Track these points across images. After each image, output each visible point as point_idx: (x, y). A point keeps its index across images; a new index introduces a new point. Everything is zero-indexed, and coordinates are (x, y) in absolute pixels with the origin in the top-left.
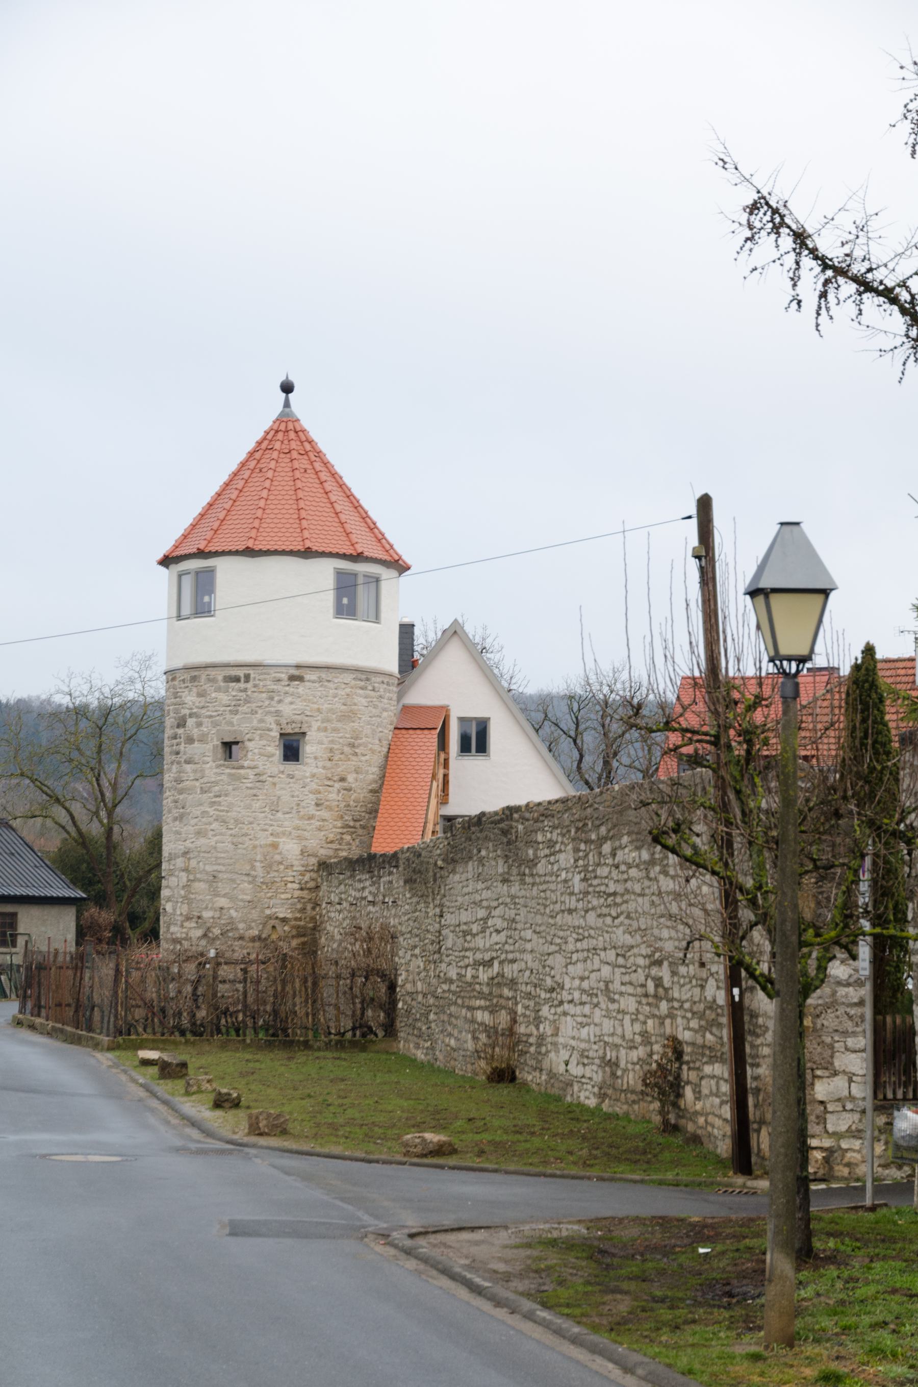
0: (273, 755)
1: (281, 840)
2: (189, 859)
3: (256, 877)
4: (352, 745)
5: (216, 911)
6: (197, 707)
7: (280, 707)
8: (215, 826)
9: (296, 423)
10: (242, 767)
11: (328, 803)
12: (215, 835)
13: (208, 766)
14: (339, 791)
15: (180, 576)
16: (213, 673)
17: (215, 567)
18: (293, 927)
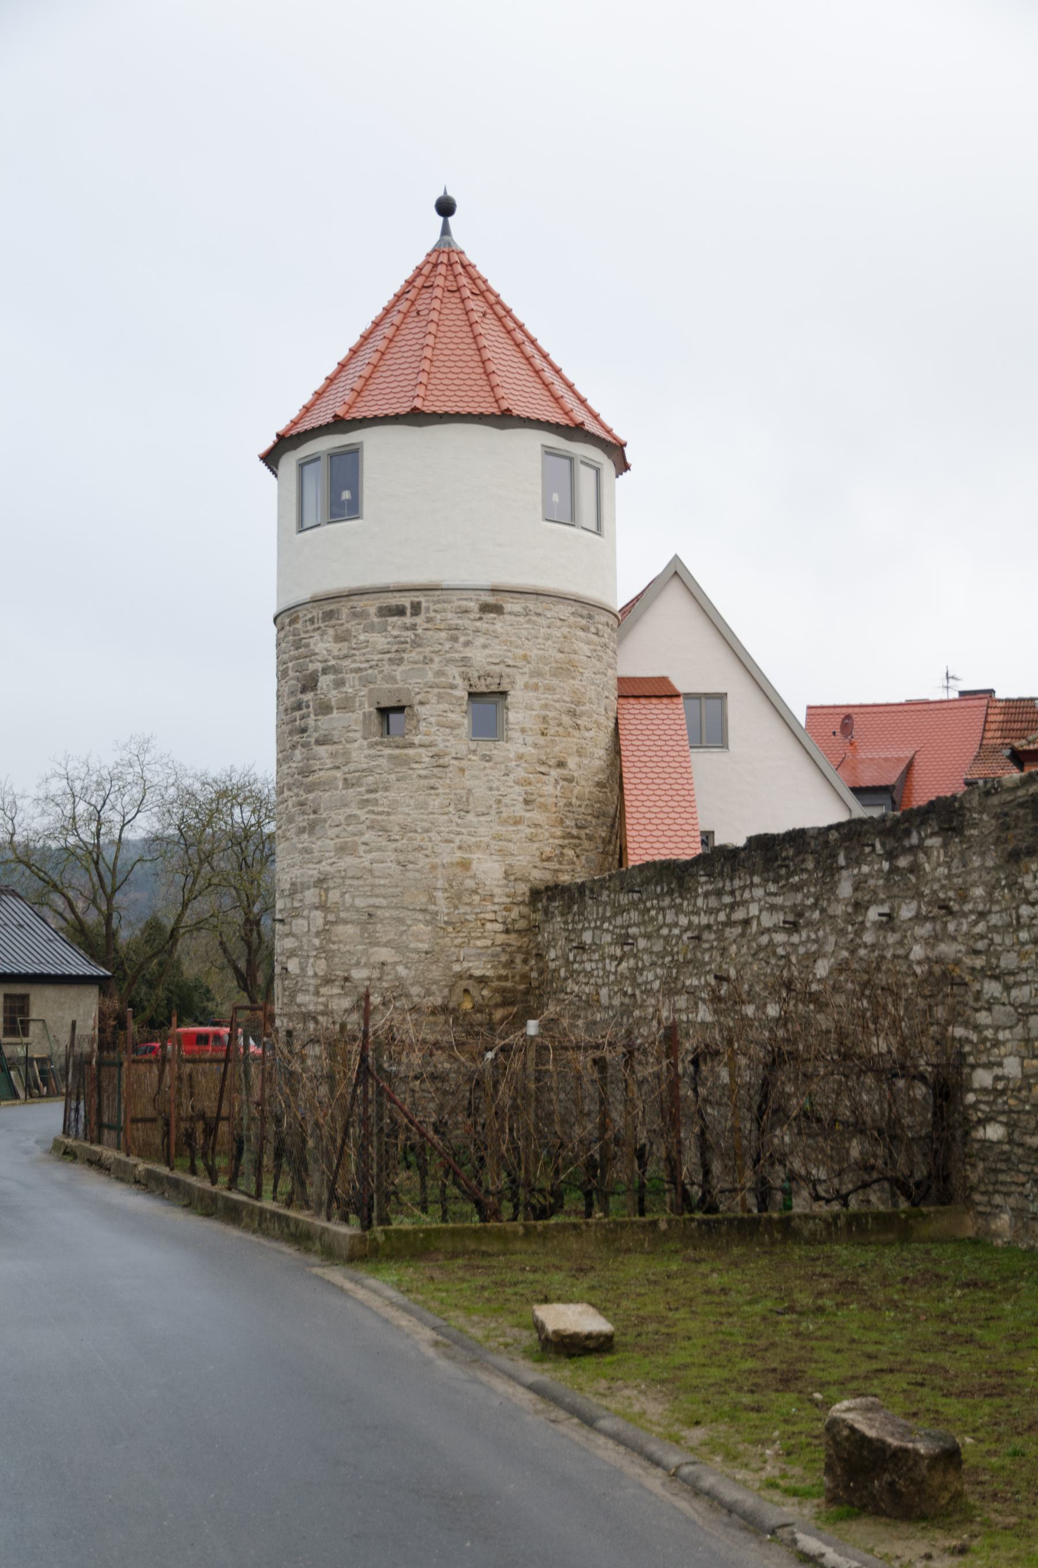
0: (459, 726)
1: (474, 856)
2: (327, 890)
3: (437, 913)
4: (573, 714)
5: (374, 968)
6: (338, 658)
7: (468, 652)
8: (368, 836)
9: (462, 256)
10: (412, 745)
11: (542, 800)
12: (370, 851)
13: (356, 745)
14: (557, 782)
15: (302, 466)
16: (361, 604)
17: (361, 443)
18: (496, 990)
